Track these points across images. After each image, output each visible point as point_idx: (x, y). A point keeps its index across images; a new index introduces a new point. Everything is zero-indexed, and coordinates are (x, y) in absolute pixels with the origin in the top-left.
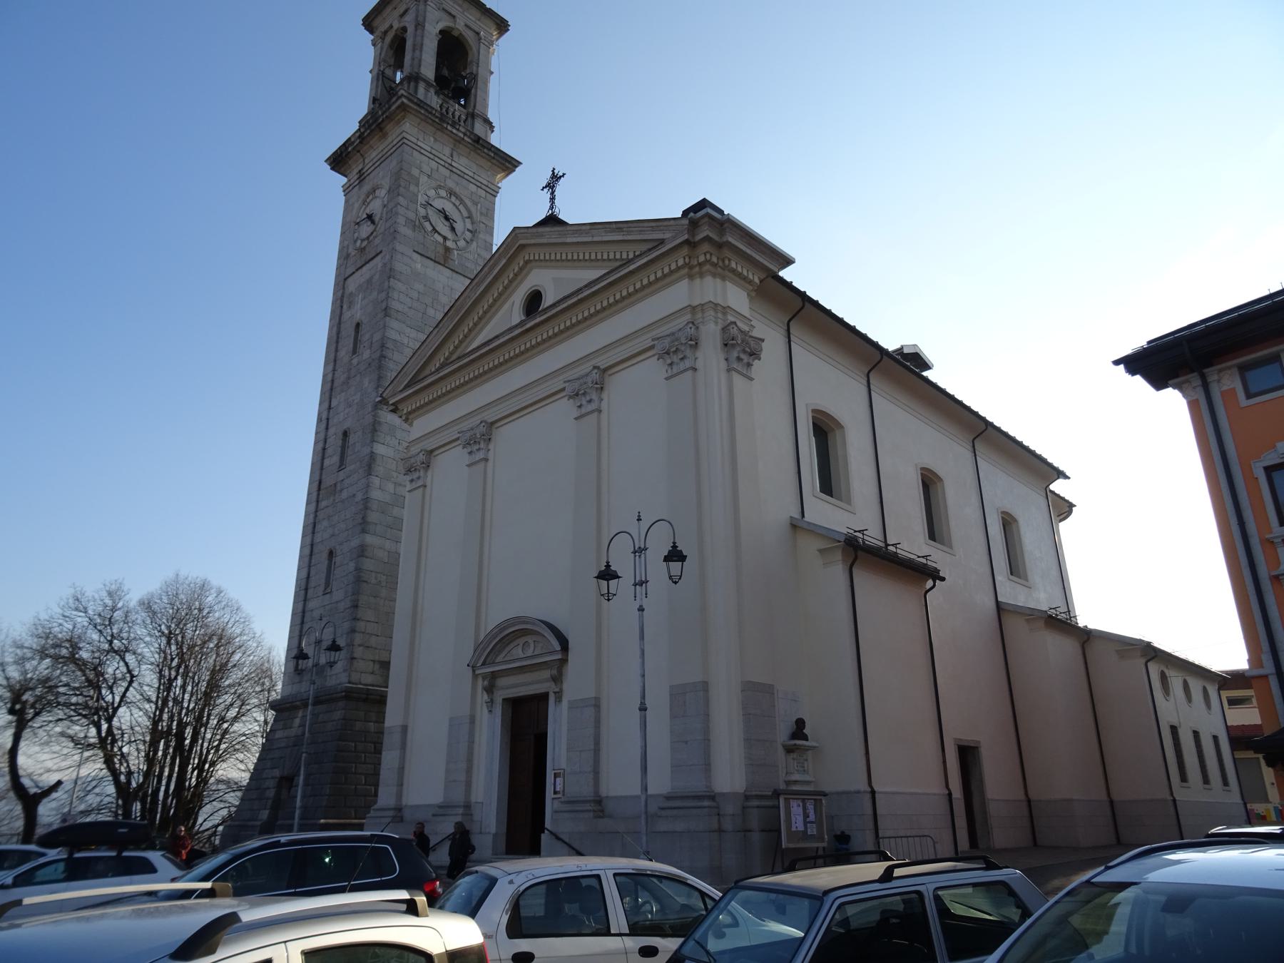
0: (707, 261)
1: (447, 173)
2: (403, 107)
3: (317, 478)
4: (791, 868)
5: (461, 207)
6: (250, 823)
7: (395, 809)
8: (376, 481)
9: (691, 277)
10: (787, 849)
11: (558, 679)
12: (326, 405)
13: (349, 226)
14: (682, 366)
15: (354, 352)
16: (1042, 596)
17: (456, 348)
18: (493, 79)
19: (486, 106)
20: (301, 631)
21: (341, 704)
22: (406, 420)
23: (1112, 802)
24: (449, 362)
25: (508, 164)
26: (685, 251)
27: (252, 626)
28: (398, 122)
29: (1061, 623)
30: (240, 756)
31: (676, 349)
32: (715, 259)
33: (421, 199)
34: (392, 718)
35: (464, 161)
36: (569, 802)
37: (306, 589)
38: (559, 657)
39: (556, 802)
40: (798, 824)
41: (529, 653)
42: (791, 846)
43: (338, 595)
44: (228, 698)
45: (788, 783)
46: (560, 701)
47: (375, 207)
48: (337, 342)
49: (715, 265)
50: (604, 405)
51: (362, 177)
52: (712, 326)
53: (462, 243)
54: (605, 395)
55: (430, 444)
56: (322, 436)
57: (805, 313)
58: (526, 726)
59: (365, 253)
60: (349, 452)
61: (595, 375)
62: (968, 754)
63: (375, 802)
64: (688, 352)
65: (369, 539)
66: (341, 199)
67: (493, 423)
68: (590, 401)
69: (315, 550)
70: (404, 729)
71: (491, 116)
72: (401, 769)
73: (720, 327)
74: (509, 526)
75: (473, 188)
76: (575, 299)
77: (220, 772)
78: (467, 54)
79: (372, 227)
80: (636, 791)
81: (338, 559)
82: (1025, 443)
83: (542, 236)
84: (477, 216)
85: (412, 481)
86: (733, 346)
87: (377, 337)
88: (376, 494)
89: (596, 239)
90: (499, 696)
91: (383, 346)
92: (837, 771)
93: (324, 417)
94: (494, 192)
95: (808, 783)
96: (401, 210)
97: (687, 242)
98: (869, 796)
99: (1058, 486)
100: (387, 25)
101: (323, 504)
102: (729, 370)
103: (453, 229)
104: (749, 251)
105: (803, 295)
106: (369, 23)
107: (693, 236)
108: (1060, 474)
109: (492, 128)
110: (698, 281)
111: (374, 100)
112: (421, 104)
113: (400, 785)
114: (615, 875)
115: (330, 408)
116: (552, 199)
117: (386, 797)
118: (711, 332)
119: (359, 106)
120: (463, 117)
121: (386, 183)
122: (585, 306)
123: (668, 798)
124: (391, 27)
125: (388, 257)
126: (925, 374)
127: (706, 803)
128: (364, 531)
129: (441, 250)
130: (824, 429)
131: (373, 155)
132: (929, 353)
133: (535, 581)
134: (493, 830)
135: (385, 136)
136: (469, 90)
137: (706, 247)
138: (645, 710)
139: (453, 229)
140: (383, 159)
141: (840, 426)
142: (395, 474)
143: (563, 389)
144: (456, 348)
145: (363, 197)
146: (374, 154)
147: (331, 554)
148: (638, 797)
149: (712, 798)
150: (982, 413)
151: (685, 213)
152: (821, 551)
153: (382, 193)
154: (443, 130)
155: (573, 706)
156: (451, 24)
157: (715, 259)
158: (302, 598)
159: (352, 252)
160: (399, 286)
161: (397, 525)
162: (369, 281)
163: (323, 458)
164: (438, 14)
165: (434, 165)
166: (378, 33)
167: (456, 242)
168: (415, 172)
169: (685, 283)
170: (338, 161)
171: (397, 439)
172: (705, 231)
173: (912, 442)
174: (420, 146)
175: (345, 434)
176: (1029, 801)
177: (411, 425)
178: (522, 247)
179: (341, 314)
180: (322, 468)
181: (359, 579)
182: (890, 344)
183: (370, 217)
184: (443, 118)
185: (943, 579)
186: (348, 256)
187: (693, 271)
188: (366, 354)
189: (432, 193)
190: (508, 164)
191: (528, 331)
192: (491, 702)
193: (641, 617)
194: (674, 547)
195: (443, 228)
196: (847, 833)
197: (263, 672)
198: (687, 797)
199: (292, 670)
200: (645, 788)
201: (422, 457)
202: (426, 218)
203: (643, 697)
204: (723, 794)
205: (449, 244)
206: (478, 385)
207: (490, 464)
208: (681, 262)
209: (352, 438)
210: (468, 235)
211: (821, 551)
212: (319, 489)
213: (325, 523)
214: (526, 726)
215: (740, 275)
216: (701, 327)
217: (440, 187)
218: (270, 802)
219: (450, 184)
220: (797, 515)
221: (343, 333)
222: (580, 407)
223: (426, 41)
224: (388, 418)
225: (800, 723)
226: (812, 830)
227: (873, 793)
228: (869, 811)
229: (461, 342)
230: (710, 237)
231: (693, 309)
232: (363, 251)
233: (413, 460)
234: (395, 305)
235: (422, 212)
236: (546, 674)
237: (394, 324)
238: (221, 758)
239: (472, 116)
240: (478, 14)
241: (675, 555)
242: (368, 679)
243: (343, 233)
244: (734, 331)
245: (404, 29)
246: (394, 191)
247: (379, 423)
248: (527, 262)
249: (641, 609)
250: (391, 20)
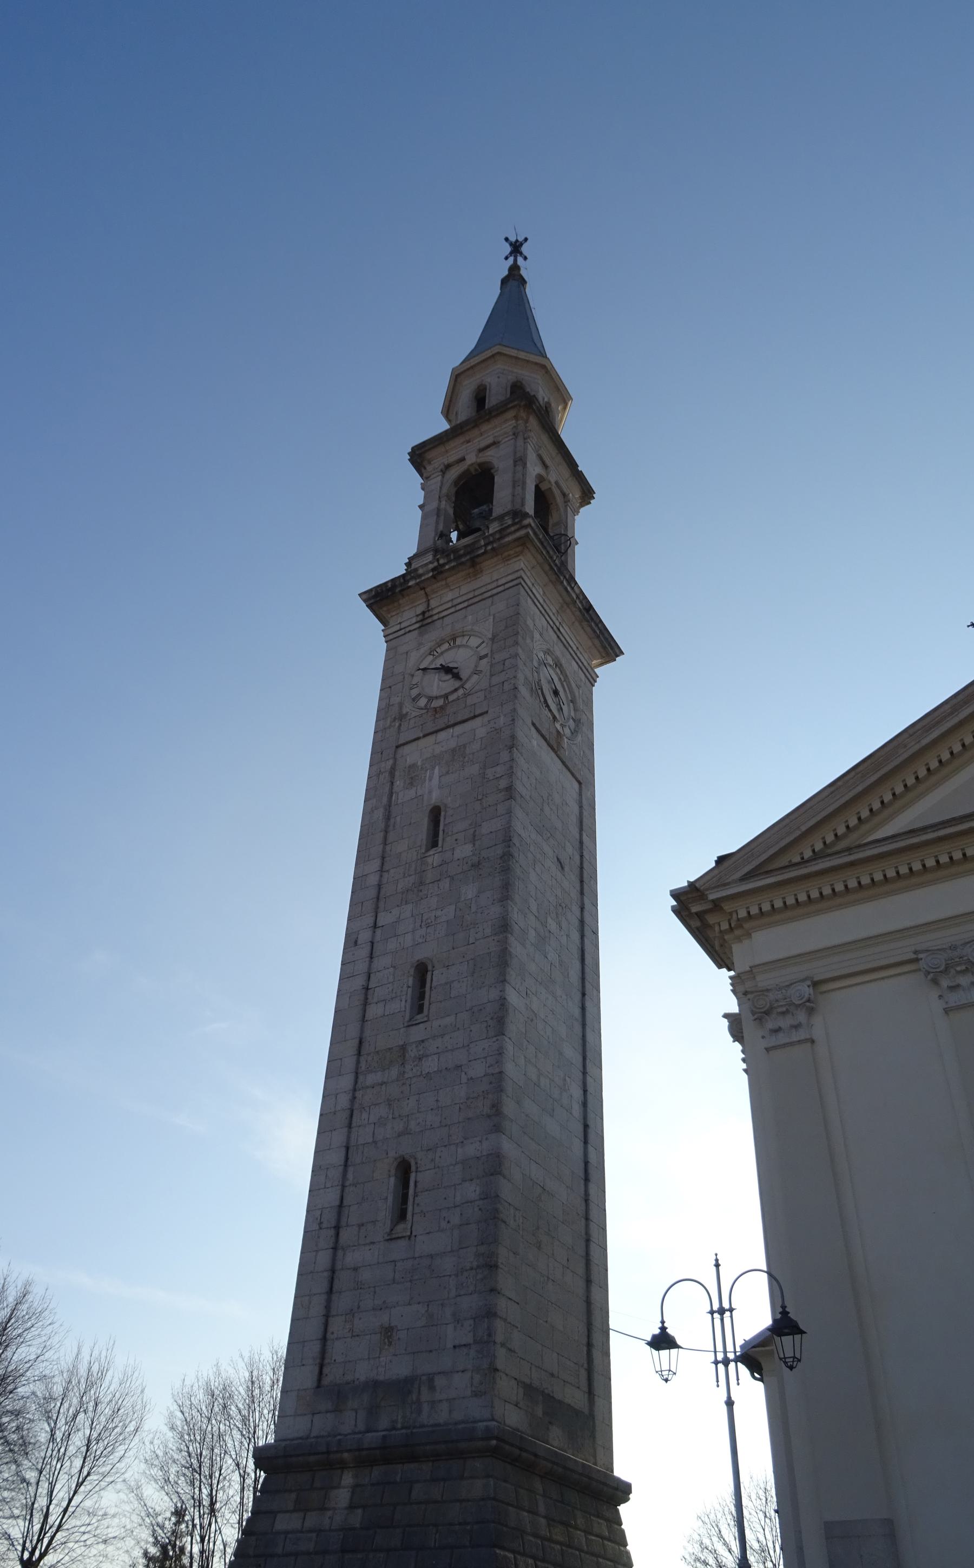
14: (795, 1037)
15: (433, 842)
20: (328, 1307)
28: (508, 558)
51: (425, 621)
68: (797, 1027)
100: (452, 458)
146: (450, 596)
147: (404, 1169)
163: (365, 1003)
170: (381, 599)
175: (422, 971)
180: (363, 1020)
209: (438, 977)
212: (359, 1054)
219: (558, 653)
234: (519, 787)
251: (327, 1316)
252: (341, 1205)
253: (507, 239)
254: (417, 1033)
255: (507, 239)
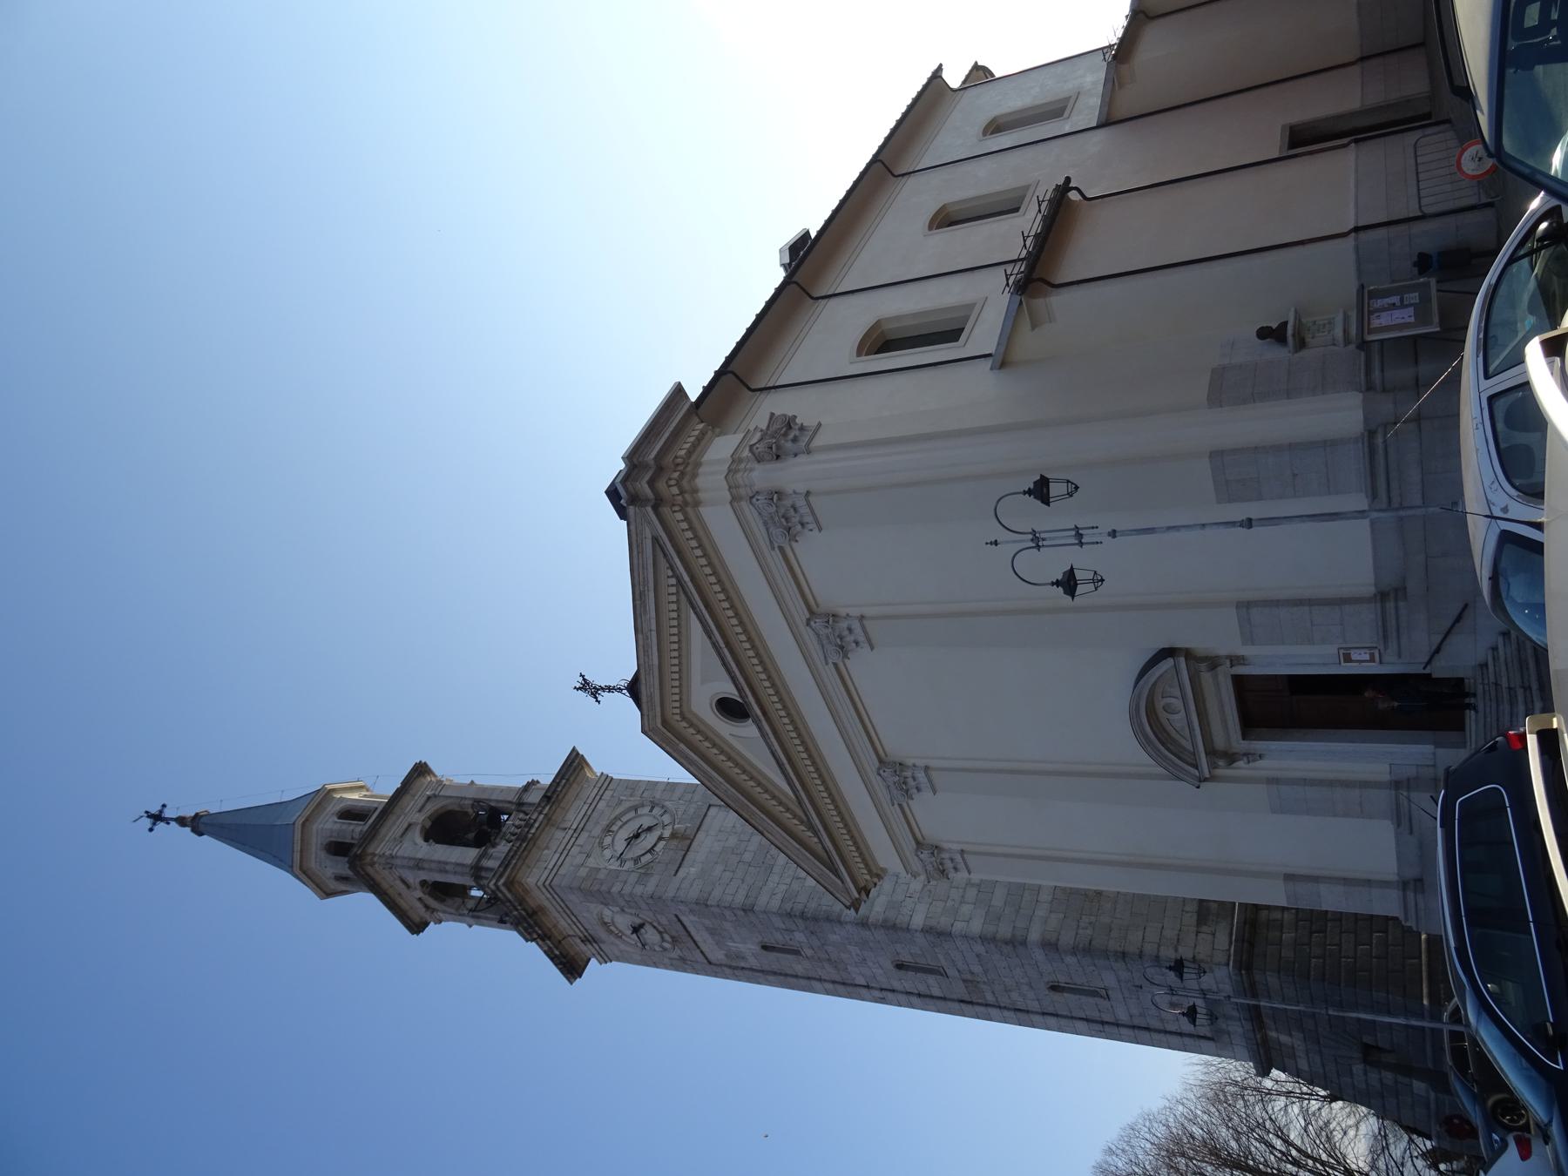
0: (678, 484)
1: (585, 835)
2: (510, 884)
3: (956, 1006)
4: (1466, 94)
5: (624, 819)
6: (1433, 1106)
7: (1404, 890)
8: (959, 927)
9: (697, 504)
10: (1441, 323)
11: (1213, 663)
12: (864, 991)
13: (648, 957)
14: (804, 510)
15: (796, 952)
16: (1089, 79)
17: (788, 810)
18: (479, 781)
19: (509, 789)
21: (1258, 977)
22: (879, 877)
23: (1362, 59)
24: (806, 821)
25: (574, 764)
26: (665, 510)
27: (1155, 1110)
28: (527, 891)
29: (1122, 53)
30: (1338, 1135)
31: (784, 519)
32: (676, 475)
33: (614, 865)
34: (1273, 895)
35: (571, 816)
36: (1385, 637)
37: (1103, 1023)
38: (1182, 659)
39: (1386, 658)
40: (1406, 315)
41: (1178, 704)
42: (1436, 319)
43: (1109, 979)
44: (1257, 1147)
45: (1347, 341)
46: (1243, 658)
47: (623, 922)
48: (786, 975)
49: (683, 474)
50: (855, 612)
51: (589, 939)
52: (755, 474)
53: (666, 819)
54: (842, 612)
55: (909, 845)
56: (902, 998)
57: (740, 372)
58: (1284, 706)
59: (680, 937)
60: (922, 961)
61: (818, 624)
62: (1304, 139)
63: (1396, 919)
64: (787, 502)
65: (1034, 936)
66: (615, 966)
67: (881, 761)
68: (850, 630)
69: (1051, 1010)
70: (1289, 877)
71: (520, 783)
72: (1346, 881)
73: (756, 465)
74: (1010, 733)
75: (602, 805)
76: (726, 651)
77: (1361, 1164)
78: (450, 813)
79: (647, 927)
80: (1362, 527)
81: (1062, 979)
82: (898, 116)
83: (651, 697)
84: (635, 800)
85: (956, 869)
86: (778, 448)
87: (778, 922)
88: (976, 927)
89: (654, 627)
90: (1239, 744)
91: (790, 915)
92: (1328, 281)
93: (877, 994)
94: (608, 780)
95: (1346, 319)
96: (627, 889)
97: (656, 508)
98: (1363, 235)
99: (954, 78)
100: (418, 905)
101: (990, 998)
102: (809, 452)
103: (650, 829)
104: (667, 435)
105: (719, 375)
106: (416, 927)
107: (648, 500)
108: (937, 75)
109: (531, 784)
110: (702, 496)
111: (502, 922)
112: (505, 864)
113: (1368, 883)
114: (1487, 377)
115: (867, 987)
116: (610, 689)
117: (1386, 904)
118: (763, 476)
119: (509, 939)
120: (521, 816)
121: (595, 908)
122: (736, 643)
123: (1374, 496)
124: (420, 899)
125: (682, 907)
126: (813, 235)
127: (1379, 440)
128: (1024, 943)
129: (675, 842)
130: (880, 341)
131: (564, 924)
132: (790, 234)
133: (1083, 702)
134: (1429, 748)
135: (541, 909)
136: (492, 808)
137: (661, 485)
138: (1250, 520)
139: (650, 829)
140: (568, 911)
141: (878, 324)
142: (950, 903)
143: (835, 665)
144: (788, 810)
145: (612, 938)
147: (1055, 988)
148: (1372, 523)
149: (1371, 434)
150: (862, 167)
151: (622, 513)
152: (1034, 327)
153: (607, 914)
154: (535, 839)
155: (1249, 639)
156: (418, 828)
157: (676, 475)
158: (1115, 1030)
159: (676, 953)
160: (717, 893)
161: (1017, 892)
162: (712, 932)
163: (932, 997)
164: (407, 844)
165: (575, 850)
166: (427, 916)
167: (664, 826)
168: (583, 872)
169: (704, 511)
170: (572, 968)
171: (902, 893)
172: (643, 487)
173: (899, 239)
174: (552, 866)
175: (900, 966)
176: (1362, 59)
177: (884, 870)
178: (665, 722)
179: (751, 969)
180: (944, 999)
181: (1086, 950)
182: (779, 276)
183: (636, 930)
184: (522, 838)
185: (1068, 180)
186: (683, 959)
187: (690, 502)
188: (800, 937)
189: (607, 853)
190: (574, 764)
191: (765, 713)
192: (1250, 756)
193: (1124, 533)
194: (1029, 492)
195: (648, 840)
196: (1415, 259)
197: (1219, 1096)
198: (1373, 475)
199: (1211, 1044)
200: (1361, 514)
201: (925, 855)
202: (637, 860)
203: (1233, 524)
204: (1366, 420)
205: (667, 834)
206: (836, 785)
207: (932, 763)
208: (680, 516)
209: (906, 958)
210: (657, 811)
211: (1034, 327)
212: (971, 1003)
213: (1015, 995)
214: (1284, 706)
215: (694, 446)
216: (756, 488)
217: (601, 843)
218: (1400, 1078)
219: (597, 831)
220: (988, 363)
221: (775, 967)
222: (857, 643)
223: (436, 857)
224: (877, 906)
225: (1264, 333)
226: (1414, 297)
227: (1357, 229)
228: (1382, 232)
229: (781, 803)
230: (654, 481)
231: (735, 499)
232: (677, 939)
233: (929, 868)
234: (740, 899)
235: (629, 865)
236: (1206, 678)
237: (762, 901)
238: (1340, 1161)
239: (520, 805)
240: (407, 798)
241: (1041, 489)
242: (1222, 940)
243: (655, 965)
244: (761, 447)
245: (423, 883)
246: (605, 898)
247: (885, 921)
248: (684, 718)
249: (1113, 534)
250: (413, 899)
251: (1166, 1032)
252: (1086, 1020)
253: (151, 830)
254: (951, 972)
255: (151, 830)
